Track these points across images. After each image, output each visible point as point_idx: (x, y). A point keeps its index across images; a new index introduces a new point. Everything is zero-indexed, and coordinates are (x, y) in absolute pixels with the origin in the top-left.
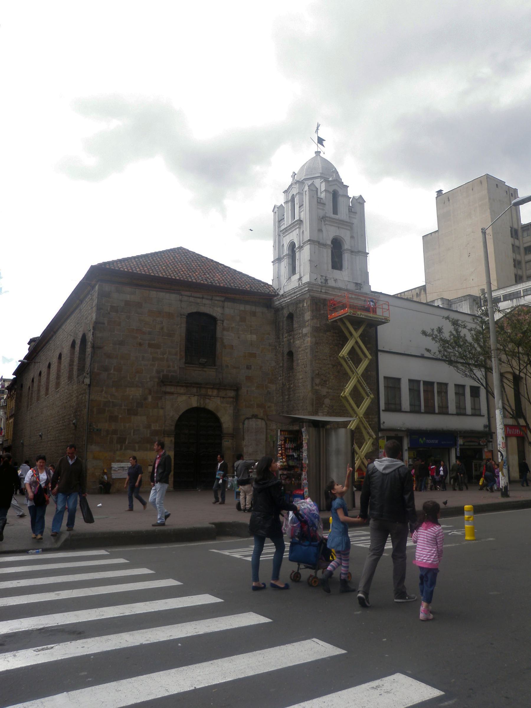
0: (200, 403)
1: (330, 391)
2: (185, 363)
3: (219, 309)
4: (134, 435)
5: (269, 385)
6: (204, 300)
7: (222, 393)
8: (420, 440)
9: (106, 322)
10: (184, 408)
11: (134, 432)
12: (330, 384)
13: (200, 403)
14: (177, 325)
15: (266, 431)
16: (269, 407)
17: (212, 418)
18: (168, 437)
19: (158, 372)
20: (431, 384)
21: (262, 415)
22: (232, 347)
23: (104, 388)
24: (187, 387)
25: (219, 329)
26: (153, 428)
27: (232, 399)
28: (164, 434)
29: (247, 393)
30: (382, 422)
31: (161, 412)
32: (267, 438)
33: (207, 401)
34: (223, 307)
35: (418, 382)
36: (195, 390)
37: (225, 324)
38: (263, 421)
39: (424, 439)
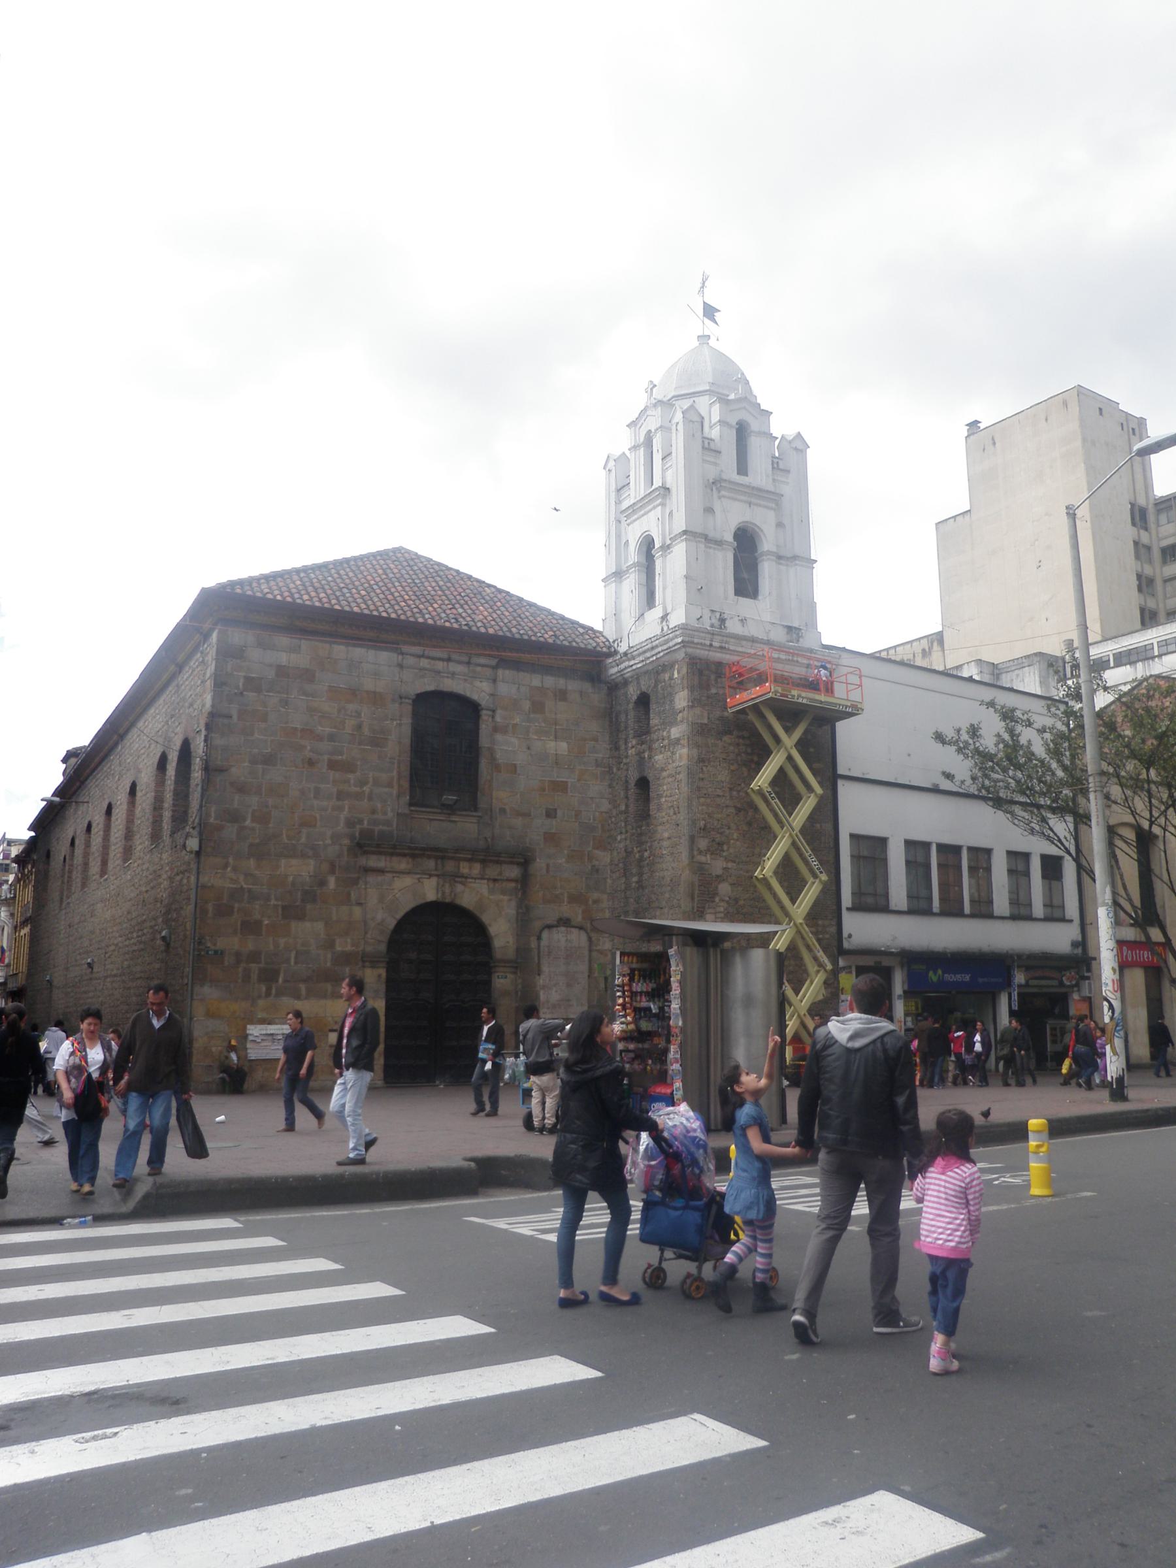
0: (443, 893)
2: (411, 804)
3: (484, 684)
5: (596, 852)
6: (451, 664)
7: (492, 871)
8: (931, 974)
9: (235, 717)
10: (407, 904)
11: (296, 957)
12: (731, 850)
13: (443, 893)
16: (595, 902)
19: (350, 823)
20: (955, 850)
22: (513, 769)
24: (413, 856)
25: (485, 727)
26: (338, 948)
30: (845, 935)
33: (459, 888)
34: (495, 681)
35: (926, 845)
36: (430, 864)
37: (498, 719)
39: (940, 972)
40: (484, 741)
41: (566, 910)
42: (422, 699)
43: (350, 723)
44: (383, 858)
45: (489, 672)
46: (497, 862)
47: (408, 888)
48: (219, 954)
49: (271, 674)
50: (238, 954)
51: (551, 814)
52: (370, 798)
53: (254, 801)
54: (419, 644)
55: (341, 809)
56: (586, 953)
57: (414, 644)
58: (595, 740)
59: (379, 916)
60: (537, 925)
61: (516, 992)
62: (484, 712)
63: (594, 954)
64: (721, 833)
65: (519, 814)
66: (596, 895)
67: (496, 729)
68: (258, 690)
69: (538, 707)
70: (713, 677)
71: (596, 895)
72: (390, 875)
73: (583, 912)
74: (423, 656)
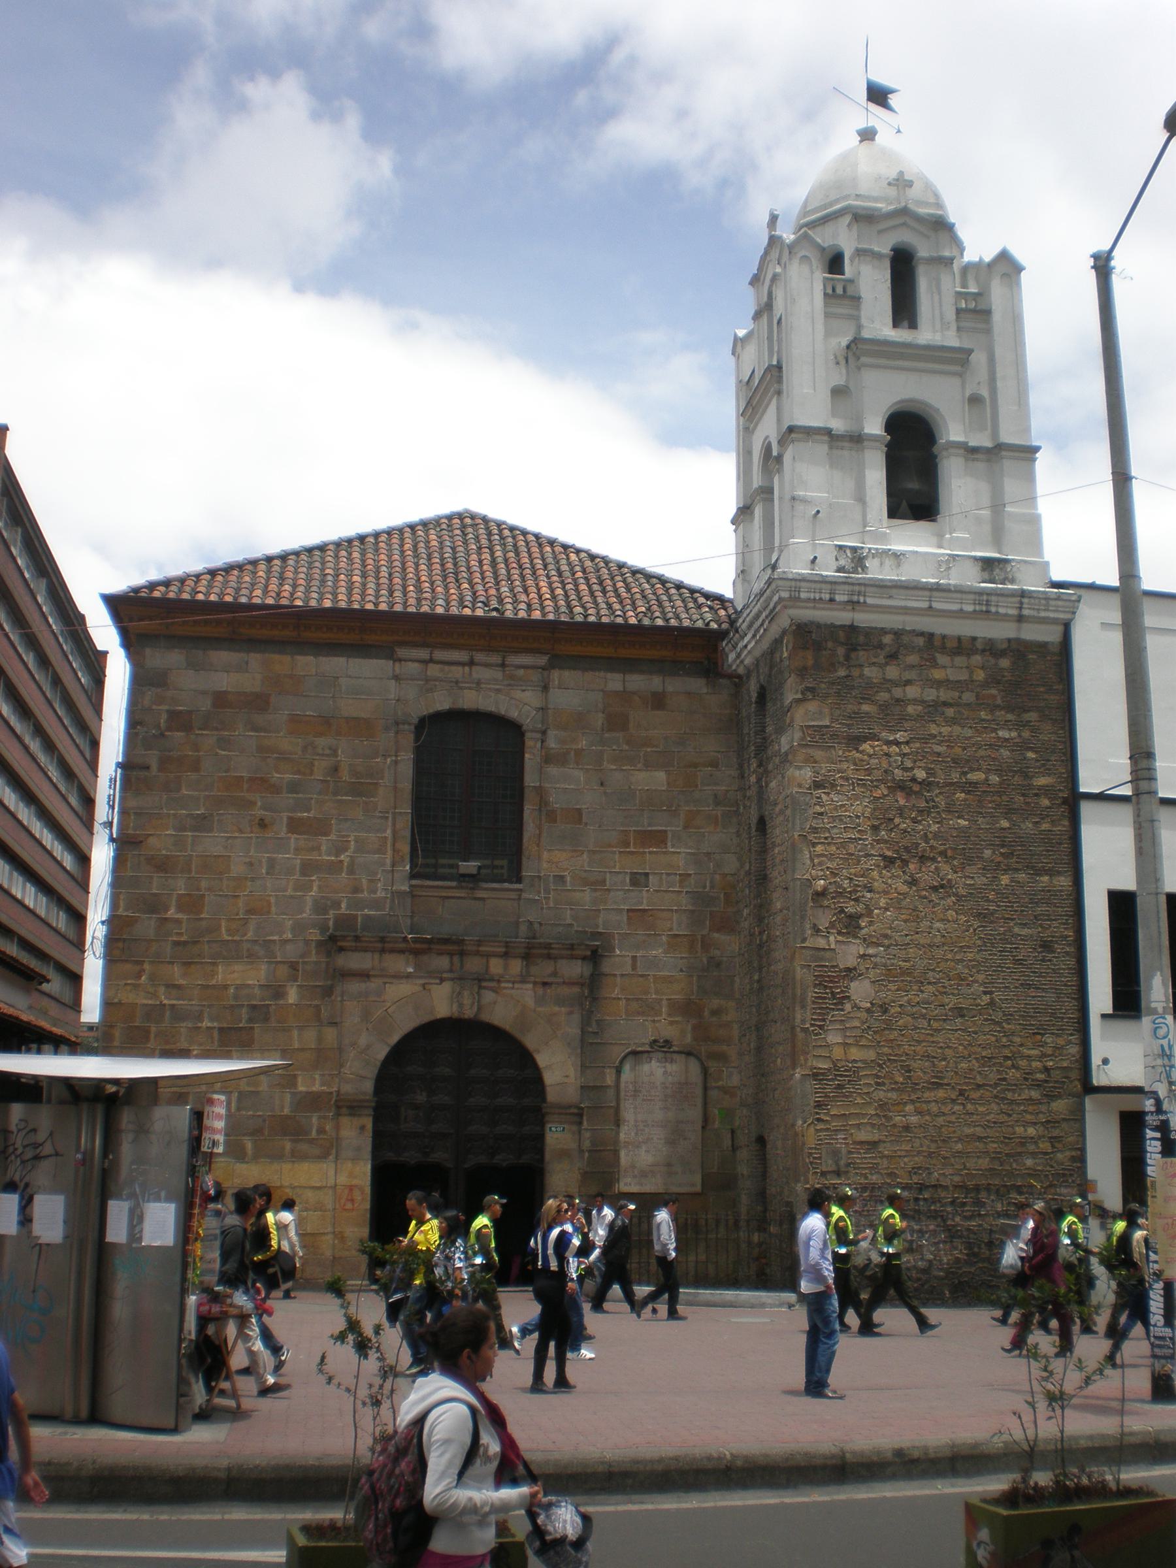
0: (461, 1005)
2: (413, 876)
3: (527, 694)
5: (716, 935)
6: (474, 668)
7: (543, 969)
9: (154, 767)
10: (405, 1024)
13: (461, 1005)
14: (385, 756)
16: (715, 1013)
17: (510, 1056)
18: (350, 1115)
19: (320, 908)
22: (577, 816)
24: (416, 953)
25: (531, 759)
26: (301, 1088)
28: (338, 1107)
30: (1096, 1060)
33: (488, 996)
34: (545, 688)
36: (443, 962)
37: (552, 744)
40: (530, 779)
42: (422, 720)
43: (321, 767)
44: (369, 955)
45: (535, 676)
46: (549, 957)
47: (411, 996)
49: (206, 704)
52: (351, 871)
53: (180, 886)
54: (424, 645)
55: (307, 887)
56: (699, 1091)
57: (415, 645)
58: (714, 764)
59: (363, 1041)
60: (618, 1052)
61: (581, 1151)
62: (528, 735)
63: (713, 1094)
64: (857, 900)
66: (716, 1003)
67: (548, 759)
68: (187, 728)
69: (616, 722)
70: (841, 651)
71: (716, 1003)
72: (380, 981)
73: (694, 1028)
74: (431, 661)
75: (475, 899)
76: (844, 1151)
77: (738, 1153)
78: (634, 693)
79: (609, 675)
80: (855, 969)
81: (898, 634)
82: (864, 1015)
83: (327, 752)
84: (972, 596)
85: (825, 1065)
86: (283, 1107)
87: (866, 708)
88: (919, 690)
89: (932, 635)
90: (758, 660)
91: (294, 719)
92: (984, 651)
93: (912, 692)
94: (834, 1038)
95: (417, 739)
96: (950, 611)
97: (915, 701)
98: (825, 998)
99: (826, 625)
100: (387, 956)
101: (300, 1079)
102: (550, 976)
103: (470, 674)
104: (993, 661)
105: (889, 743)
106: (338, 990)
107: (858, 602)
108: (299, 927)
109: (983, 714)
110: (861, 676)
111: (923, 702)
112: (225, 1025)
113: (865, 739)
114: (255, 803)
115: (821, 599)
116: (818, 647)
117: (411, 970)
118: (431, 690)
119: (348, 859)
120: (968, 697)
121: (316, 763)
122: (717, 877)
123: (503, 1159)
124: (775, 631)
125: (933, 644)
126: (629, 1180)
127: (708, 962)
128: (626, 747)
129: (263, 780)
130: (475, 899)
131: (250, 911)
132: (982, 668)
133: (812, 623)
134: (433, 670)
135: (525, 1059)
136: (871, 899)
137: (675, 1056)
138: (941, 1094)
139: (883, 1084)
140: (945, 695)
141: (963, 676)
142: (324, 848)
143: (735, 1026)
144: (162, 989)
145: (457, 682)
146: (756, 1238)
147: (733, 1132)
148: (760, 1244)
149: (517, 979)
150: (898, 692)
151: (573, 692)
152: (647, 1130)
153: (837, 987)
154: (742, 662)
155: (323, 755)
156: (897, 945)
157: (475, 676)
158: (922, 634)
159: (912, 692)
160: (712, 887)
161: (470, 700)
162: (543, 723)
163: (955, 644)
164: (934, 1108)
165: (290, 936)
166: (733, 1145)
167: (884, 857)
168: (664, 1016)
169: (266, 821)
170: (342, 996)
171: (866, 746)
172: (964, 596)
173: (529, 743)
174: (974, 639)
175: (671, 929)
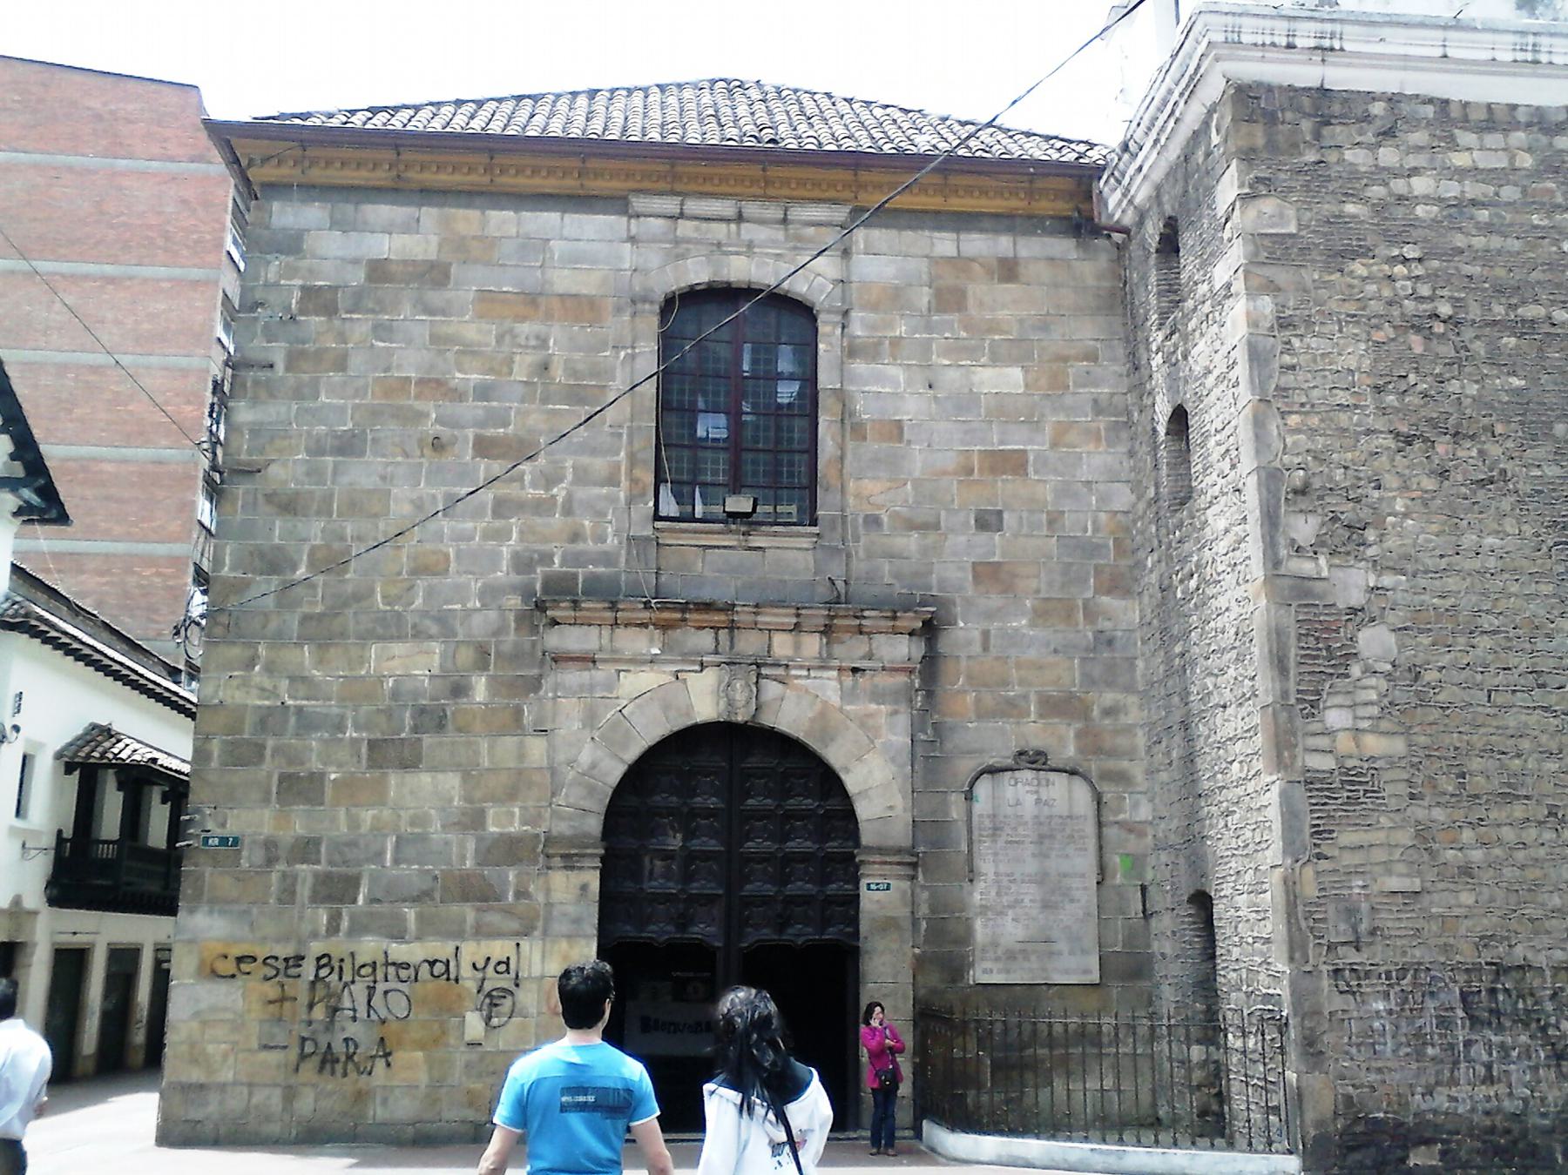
1: (1388, 580)
4: (396, 861)
5: (1105, 599)
6: (744, 226)
7: (852, 650)
10: (650, 730)
11: (398, 846)
12: (1391, 542)
15: (1100, 836)
16: (1109, 712)
19: (523, 563)
21: (1071, 751)
22: (896, 430)
23: (262, 650)
25: (827, 349)
26: (493, 829)
27: (902, 679)
29: (986, 648)
31: (537, 749)
32: (1102, 869)
33: (771, 689)
34: (846, 253)
36: (705, 639)
37: (857, 330)
38: (1077, 781)
41: (1034, 732)
44: (594, 630)
48: (231, 843)
49: (357, 277)
50: (270, 845)
51: (988, 522)
54: (674, 193)
55: (502, 535)
56: (1090, 828)
58: (1092, 357)
60: (966, 767)
61: (915, 923)
62: (821, 318)
63: (1111, 833)
65: (911, 526)
66: (1110, 697)
68: (330, 310)
69: (949, 299)
70: (1306, 125)
71: (1110, 697)
72: (612, 668)
73: (1079, 735)
74: (682, 216)
75: (750, 549)
76: (1364, 906)
77: (1153, 922)
78: (973, 260)
79: (936, 234)
80: (1362, 610)
81: (1393, 100)
82: (1383, 684)
83: (533, 342)
84: (1511, 38)
85: (1327, 763)
86: (463, 858)
87: (1350, 208)
88: (1432, 182)
89: (1447, 102)
90: (1158, 189)
91: (485, 296)
92: (1529, 125)
93: (1421, 185)
94: (1336, 718)
95: (663, 322)
96: (1475, 62)
97: (1427, 199)
98: (1316, 657)
99: (1280, 87)
100: (620, 632)
101: (491, 813)
102: (863, 658)
103: (739, 234)
104: (1544, 140)
105: (1393, 261)
106: (547, 683)
107: (1332, 49)
108: (490, 594)
109: (1536, 219)
110: (1341, 161)
111: (1440, 200)
112: (379, 736)
113: (1354, 255)
114: (428, 415)
115: (1273, 44)
116: (1271, 119)
117: (656, 651)
118: (682, 257)
119: (564, 493)
120: (1509, 193)
121: (517, 358)
122: (1103, 517)
123: (800, 934)
124: (1193, 115)
125: (1449, 118)
126: (988, 965)
127: (1095, 638)
128: (963, 334)
129: (439, 383)
130: (750, 549)
131: (417, 571)
132: (1529, 150)
133: (1259, 84)
134: (686, 228)
135: (829, 782)
136: (1380, 499)
137: (1052, 775)
138: (1518, 811)
139: (1421, 797)
140: (1472, 190)
141: (1500, 161)
142: (527, 478)
143: (1140, 733)
144: (284, 684)
145: (719, 245)
146: (1197, 1053)
147: (1144, 889)
148: (1204, 1064)
149: (816, 663)
150: (1399, 186)
151: (887, 259)
152: (1014, 888)
153: (1336, 640)
154: (1131, 202)
155: (527, 347)
156: (1426, 572)
157: (745, 236)
158: (1431, 101)
159: (1421, 185)
160: (1096, 529)
161: (739, 270)
162: (843, 300)
163: (1483, 115)
164: (1508, 834)
165: (478, 605)
166: (1144, 911)
167: (1397, 435)
168: (1033, 717)
169: (444, 440)
170: (555, 691)
171: (1358, 267)
172: (1497, 37)
173: (823, 329)
174: (1514, 107)
175: (1038, 591)
